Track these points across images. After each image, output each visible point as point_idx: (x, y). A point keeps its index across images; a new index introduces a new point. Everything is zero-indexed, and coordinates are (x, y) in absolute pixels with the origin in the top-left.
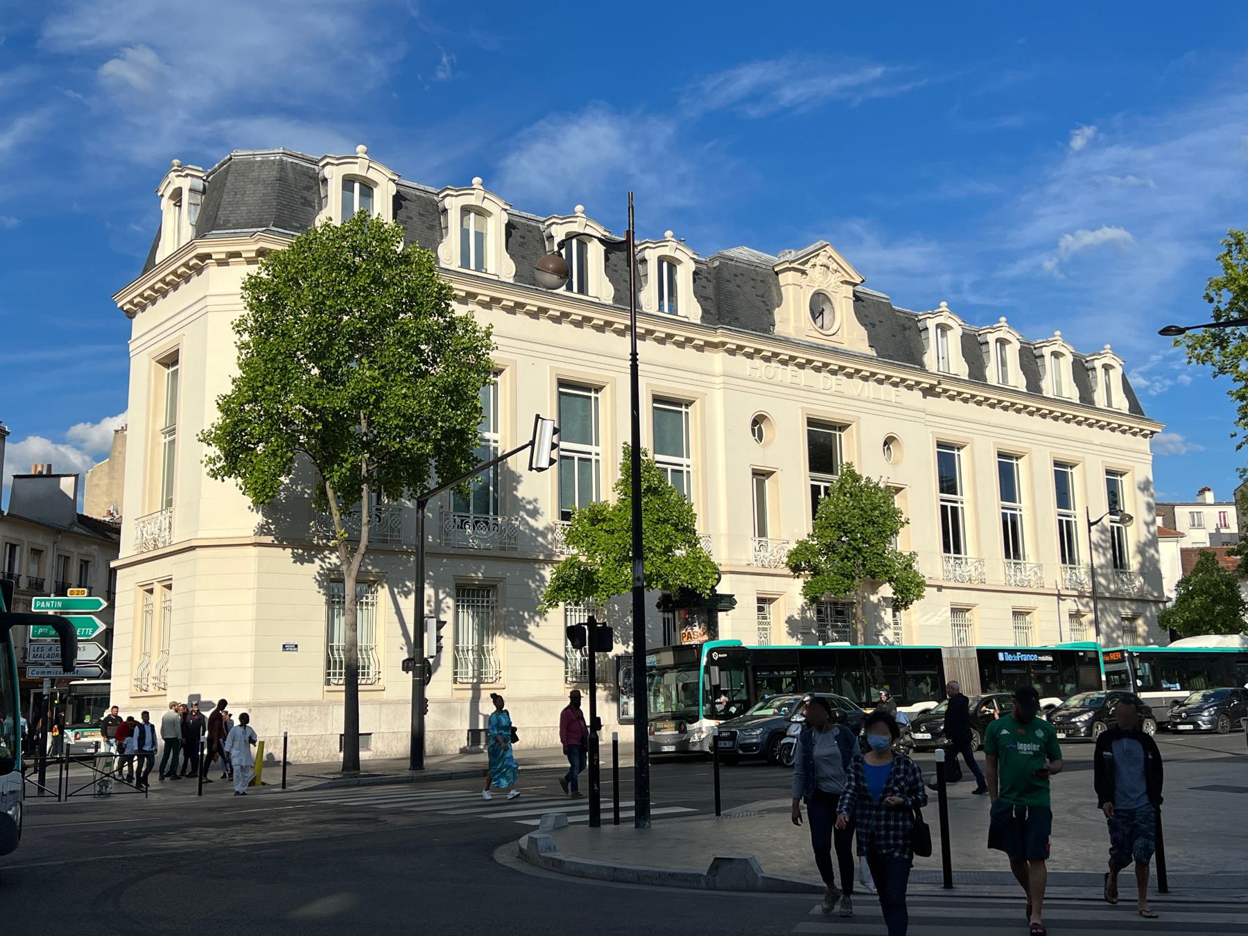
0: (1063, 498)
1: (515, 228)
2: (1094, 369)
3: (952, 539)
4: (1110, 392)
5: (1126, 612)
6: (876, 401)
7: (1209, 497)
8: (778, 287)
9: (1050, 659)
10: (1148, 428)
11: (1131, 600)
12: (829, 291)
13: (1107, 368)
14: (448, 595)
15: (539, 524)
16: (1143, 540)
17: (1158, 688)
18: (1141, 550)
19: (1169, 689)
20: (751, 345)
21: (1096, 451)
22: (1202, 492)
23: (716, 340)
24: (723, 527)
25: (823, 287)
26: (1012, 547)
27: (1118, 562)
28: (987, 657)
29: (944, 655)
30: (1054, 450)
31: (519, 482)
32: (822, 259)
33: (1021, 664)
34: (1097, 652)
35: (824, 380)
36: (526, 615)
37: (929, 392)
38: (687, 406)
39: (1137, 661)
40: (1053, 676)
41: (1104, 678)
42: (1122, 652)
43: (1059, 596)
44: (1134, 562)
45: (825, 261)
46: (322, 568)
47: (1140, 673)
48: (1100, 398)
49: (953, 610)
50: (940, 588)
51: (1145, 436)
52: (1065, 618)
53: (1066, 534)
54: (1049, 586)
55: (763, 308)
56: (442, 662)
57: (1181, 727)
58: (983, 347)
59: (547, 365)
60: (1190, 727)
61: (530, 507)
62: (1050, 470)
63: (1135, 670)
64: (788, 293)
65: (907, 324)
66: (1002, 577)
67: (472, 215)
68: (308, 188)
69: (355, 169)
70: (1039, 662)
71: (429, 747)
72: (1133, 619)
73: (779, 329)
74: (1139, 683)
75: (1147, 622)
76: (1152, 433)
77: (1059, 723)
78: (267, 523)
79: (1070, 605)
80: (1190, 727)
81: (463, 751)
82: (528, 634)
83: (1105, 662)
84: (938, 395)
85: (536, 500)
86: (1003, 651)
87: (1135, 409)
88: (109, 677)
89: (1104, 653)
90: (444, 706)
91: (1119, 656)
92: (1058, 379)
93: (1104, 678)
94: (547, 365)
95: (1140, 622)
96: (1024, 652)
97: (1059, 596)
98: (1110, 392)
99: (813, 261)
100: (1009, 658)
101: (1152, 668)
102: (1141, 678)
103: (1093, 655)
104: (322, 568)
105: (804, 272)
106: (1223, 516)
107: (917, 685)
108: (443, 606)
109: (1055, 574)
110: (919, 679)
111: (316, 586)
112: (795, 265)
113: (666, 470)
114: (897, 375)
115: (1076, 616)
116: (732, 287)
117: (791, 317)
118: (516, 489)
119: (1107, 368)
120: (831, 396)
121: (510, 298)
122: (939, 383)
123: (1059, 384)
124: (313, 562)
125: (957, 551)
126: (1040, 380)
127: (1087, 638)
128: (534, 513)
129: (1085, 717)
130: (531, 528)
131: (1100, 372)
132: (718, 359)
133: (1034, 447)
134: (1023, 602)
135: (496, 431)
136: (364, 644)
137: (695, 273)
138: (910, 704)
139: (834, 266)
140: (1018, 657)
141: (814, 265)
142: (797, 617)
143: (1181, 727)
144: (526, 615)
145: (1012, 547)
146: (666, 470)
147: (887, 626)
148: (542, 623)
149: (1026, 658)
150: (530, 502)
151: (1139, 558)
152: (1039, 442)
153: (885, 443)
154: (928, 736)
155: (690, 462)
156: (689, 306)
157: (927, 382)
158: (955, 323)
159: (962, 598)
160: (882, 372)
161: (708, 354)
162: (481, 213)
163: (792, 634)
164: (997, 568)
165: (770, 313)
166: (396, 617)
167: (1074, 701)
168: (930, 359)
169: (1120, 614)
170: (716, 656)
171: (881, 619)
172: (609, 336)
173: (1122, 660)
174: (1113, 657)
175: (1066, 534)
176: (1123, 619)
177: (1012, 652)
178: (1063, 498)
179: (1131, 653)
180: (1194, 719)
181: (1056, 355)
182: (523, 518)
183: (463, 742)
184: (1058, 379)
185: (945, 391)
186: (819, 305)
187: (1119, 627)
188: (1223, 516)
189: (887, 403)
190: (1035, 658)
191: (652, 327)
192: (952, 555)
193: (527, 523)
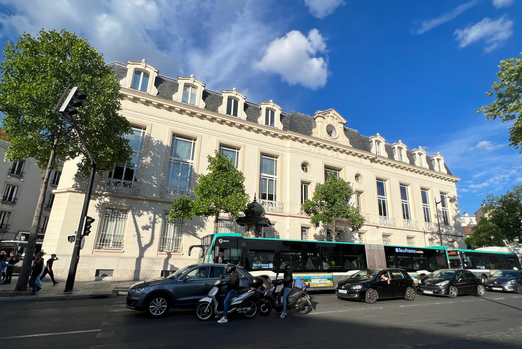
0: (425, 200)
2: (434, 160)
3: (383, 210)
4: (440, 167)
5: (451, 240)
6: (352, 161)
7: (467, 215)
8: (315, 123)
9: (422, 252)
10: (455, 179)
11: (452, 235)
12: (334, 125)
13: (438, 160)
14: (160, 217)
16: (454, 215)
17: (475, 268)
18: (455, 219)
19: (480, 269)
20: (301, 137)
21: (436, 187)
22: (464, 213)
23: (287, 135)
24: (288, 201)
25: (332, 123)
26: (406, 216)
27: (446, 223)
28: (389, 251)
29: (366, 248)
32: (331, 114)
33: (407, 254)
34: (445, 251)
35: (331, 153)
36: (196, 227)
37: (372, 160)
38: (276, 158)
39: (464, 256)
40: (423, 260)
41: (449, 262)
42: (456, 251)
43: (425, 232)
44: (452, 223)
45: (332, 115)
46: (100, 202)
47: (465, 261)
48: (436, 168)
49: (383, 235)
50: (378, 227)
51: (453, 182)
52: (427, 240)
53: (426, 212)
54: (421, 229)
55: (308, 128)
56: (154, 243)
57: (494, 289)
58: (393, 150)
60: (501, 289)
62: (419, 191)
63: (463, 259)
64: (318, 124)
65: (365, 140)
66: (402, 225)
67: (191, 88)
68: (122, 73)
69: (141, 66)
70: (416, 254)
71: (77, 278)
72: (453, 242)
74: (466, 265)
75: (458, 243)
76: (456, 181)
77: (429, 285)
78: (76, 184)
79: (429, 236)
80: (501, 289)
82: (196, 234)
83: (449, 256)
84: (376, 162)
86: (398, 247)
87: (449, 173)
88: (42, 241)
89: (449, 252)
90: (151, 260)
91: (455, 253)
92: (421, 161)
93: (449, 262)
95: (455, 243)
96: (408, 248)
97: (425, 232)
98: (440, 167)
99: (327, 114)
100: (401, 251)
101: (471, 259)
102: (466, 263)
103: (443, 252)
104: (100, 202)
105: (324, 118)
106: (471, 220)
107: (351, 262)
108: (157, 221)
109: (423, 225)
110: (351, 260)
111: (96, 209)
112: (320, 115)
114: (360, 153)
115: (431, 240)
116: (296, 121)
117: (319, 131)
119: (438, 160)
120: (335, 159)
121: (156, 101)
122: (376, 157)
123: (421, 163)
124: (96, 200)
125: (385, 215)
127: (435, 245)
129: (443, 284)
131: (436, 161)
132: (289, 143)
134: (411, 234)
135: (192, 159)
136: (119, 234)
138: (346, 271)
139: (336, 117)
140: (406, 251)
141: (328, 116)
142: (318, 234)
143: (494, 289)
144: (196, 227)
145: (406, 216)
147: (356, 239)
148: (204, 230)
149: (410, 251)
151: (454, 222)
152: (415, 182)
153: (356, 177)
154: (345, 292)
155: (277, 177)
156: (278, 124)
157: (371, 157)
158: (382, 140)
159: (387, 231)
160: (354, 151)
161: (285, 141)
162: (194, 87)
163: (315, 239)
164: (401, 222)
165: (311, 130)
166: (134, 224)
167: (436, 273)
168: (373, 150)
169: (447, 240)
170: (221, 241)
171: (353, 237)
173: (457, 255)
174: (452, 253)
175: (426, 212)
176: (449, 242)
177: (403, 248)
178: (425, 200)
179: (461, 252)
180: (502, 285)
181: (420, 154)
184: (421, 161)
185: (379, 161)
186: (330, 130)
187: (447, 244)
188: (471, 220)
189: (356, 163)
190: (414, 251)
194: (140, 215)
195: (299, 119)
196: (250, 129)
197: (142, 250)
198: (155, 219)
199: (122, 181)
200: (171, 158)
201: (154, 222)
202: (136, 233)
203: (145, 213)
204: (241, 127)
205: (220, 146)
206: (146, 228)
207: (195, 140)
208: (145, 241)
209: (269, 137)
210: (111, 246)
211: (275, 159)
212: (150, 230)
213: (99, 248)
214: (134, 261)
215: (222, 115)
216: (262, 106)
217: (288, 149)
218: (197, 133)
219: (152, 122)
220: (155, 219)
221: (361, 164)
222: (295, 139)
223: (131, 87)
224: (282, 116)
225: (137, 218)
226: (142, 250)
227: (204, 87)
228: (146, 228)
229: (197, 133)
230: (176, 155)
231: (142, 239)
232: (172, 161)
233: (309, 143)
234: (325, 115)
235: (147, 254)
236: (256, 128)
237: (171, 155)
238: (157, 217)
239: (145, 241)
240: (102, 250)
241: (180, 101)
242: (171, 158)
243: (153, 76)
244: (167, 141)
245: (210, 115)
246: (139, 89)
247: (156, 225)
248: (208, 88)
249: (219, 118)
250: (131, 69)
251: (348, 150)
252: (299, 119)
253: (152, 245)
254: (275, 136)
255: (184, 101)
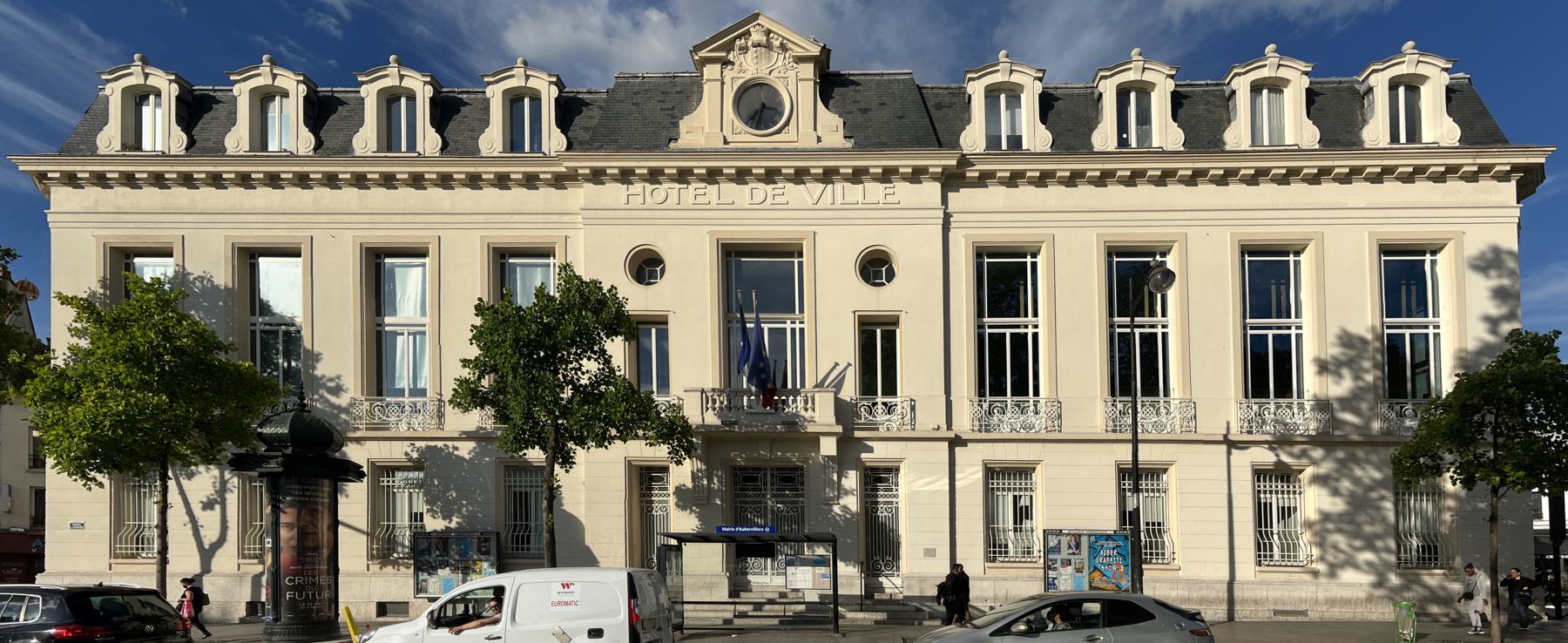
1: (1455, 91)
15: (343, 400)
16: (1472, 345)
20: (642, 164)
30: (486, 233)
31: (318, 361)
59: (1228, 232)
61: (332, 384)
67: (1265, 92)
73: (358, 152)
81: (242, 621)
85: (338, 377)
94: (1228, 232)
113: (276, 332)
118: (314, 368)
121: (1185, 167)
126: (1365, 122)
128: (337, 390)
130: (333, 406)
133: (1327, 230)
137: (1174, 94)
141: (744, 49)
142: (690, 485)
146: (276, 332)
150: (331, 380)
152: (1203, 236)
165: (676, 125)
172: (1486, 185)
182: (322, 396)
183: (242, 613)
189: (874, 207)
191: (1107, 166)
192: (1009, 398)
193: (327, 401)
194: (190, 476)
195: (637, 99)
196: (1073, 179)
197: (207, 555)
198: (224, 483)
199: (1009, 398)
200: (253, 319)
201: (222, 489)
202: (187, 519)
203: (202, 468)
204: (1043, 180)
205: (1110, 255)
206: (208, 505)
207: (1034, 255)
208: (210, 534)
209: (1144, 191)
210: (1276, 557)
211: (1292, 258)
212: (218, 507)
213: (994, 560)
214: (1225, 587)
215: (492, 160)
216: (1372, 80)
217: (579, 218)
218: (1172, 230)
219: (182, 232)
220: (224, 483)
221: (896, 207)
222: (887, 176)
223: (124, 147)
224: (1177, 100)
225: (184, 482)
226: (207, 555)
227: (1040, 79)
228: (208, 505)
229: (1172, 230)
230: (265, 309)
231: (202, 532)
232: (258, 328)
233: (1223, 180)
234: (729, 47)
235: (217, 563)
236: (1093, 168)
237: (253, 313)
238: (227, 475)
239: (210, 534)
240: (997, 564)
241: (1246, 145)
242: (253, 319)
243: (549, 94)
244: (223, 276)
245: (459, 170)
246: (527, 149)
247: (228, 496)
248: (1057, 80)
249: (488, 172)
250: (1108, 89)
251: (846, 165)
252: (637, 99)
253: (226, 545)
254: (1163, 179)
255: (993, 141)
